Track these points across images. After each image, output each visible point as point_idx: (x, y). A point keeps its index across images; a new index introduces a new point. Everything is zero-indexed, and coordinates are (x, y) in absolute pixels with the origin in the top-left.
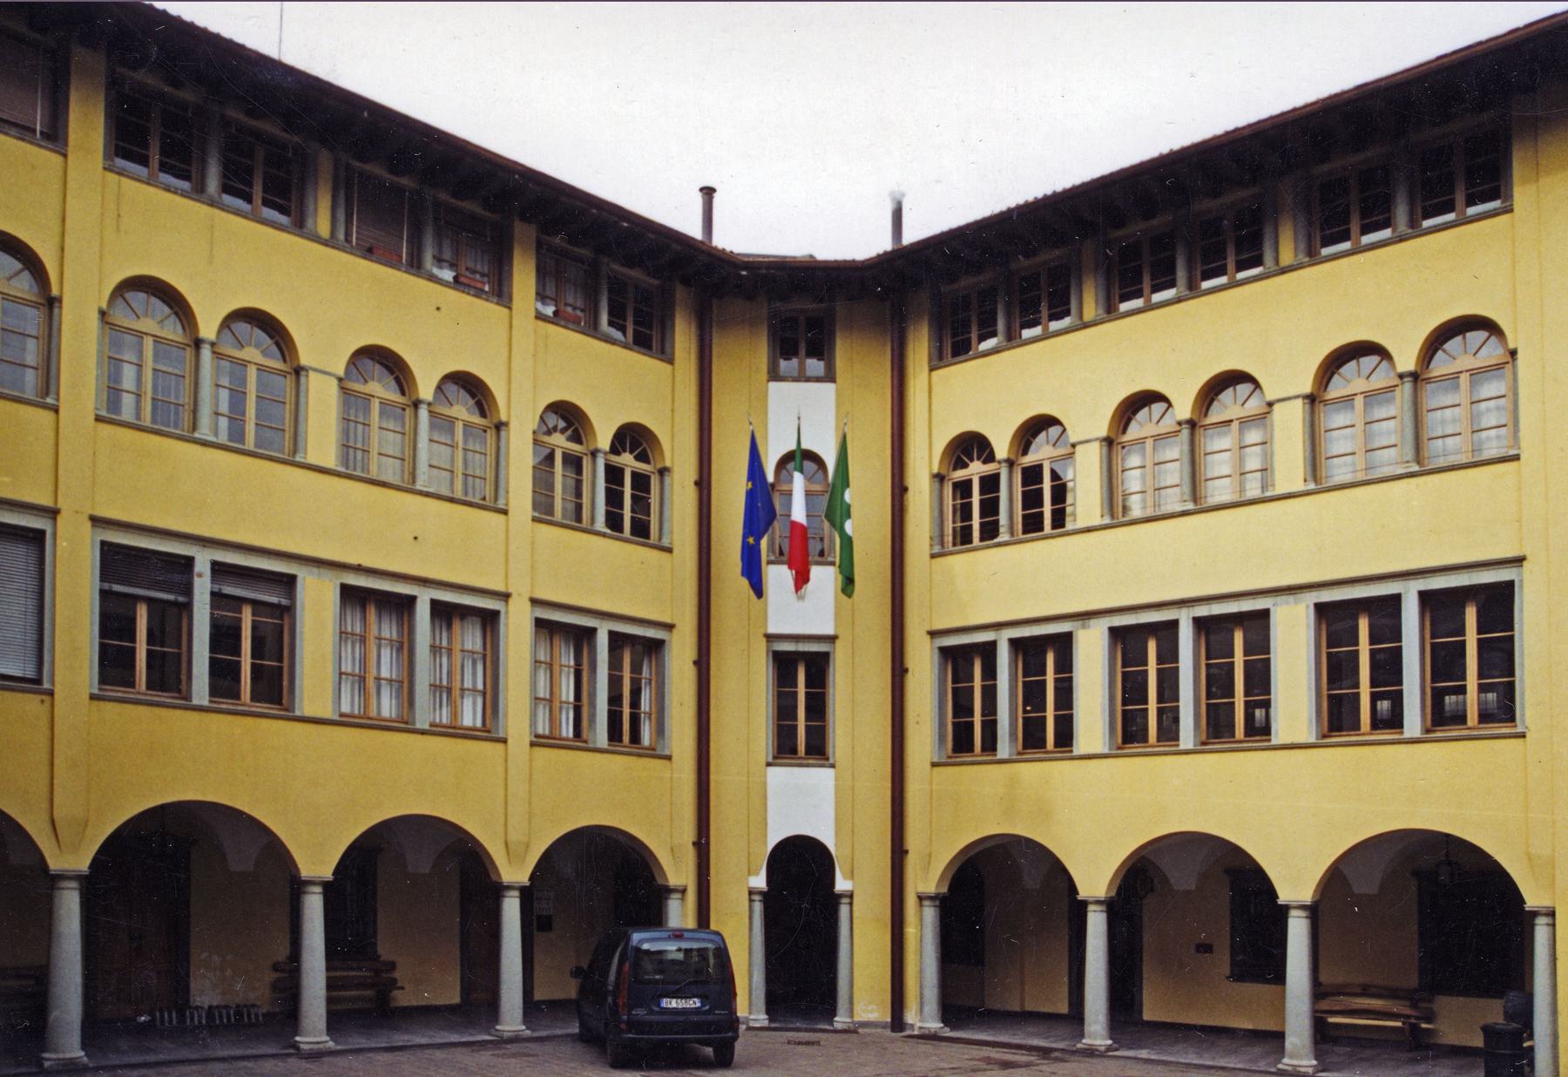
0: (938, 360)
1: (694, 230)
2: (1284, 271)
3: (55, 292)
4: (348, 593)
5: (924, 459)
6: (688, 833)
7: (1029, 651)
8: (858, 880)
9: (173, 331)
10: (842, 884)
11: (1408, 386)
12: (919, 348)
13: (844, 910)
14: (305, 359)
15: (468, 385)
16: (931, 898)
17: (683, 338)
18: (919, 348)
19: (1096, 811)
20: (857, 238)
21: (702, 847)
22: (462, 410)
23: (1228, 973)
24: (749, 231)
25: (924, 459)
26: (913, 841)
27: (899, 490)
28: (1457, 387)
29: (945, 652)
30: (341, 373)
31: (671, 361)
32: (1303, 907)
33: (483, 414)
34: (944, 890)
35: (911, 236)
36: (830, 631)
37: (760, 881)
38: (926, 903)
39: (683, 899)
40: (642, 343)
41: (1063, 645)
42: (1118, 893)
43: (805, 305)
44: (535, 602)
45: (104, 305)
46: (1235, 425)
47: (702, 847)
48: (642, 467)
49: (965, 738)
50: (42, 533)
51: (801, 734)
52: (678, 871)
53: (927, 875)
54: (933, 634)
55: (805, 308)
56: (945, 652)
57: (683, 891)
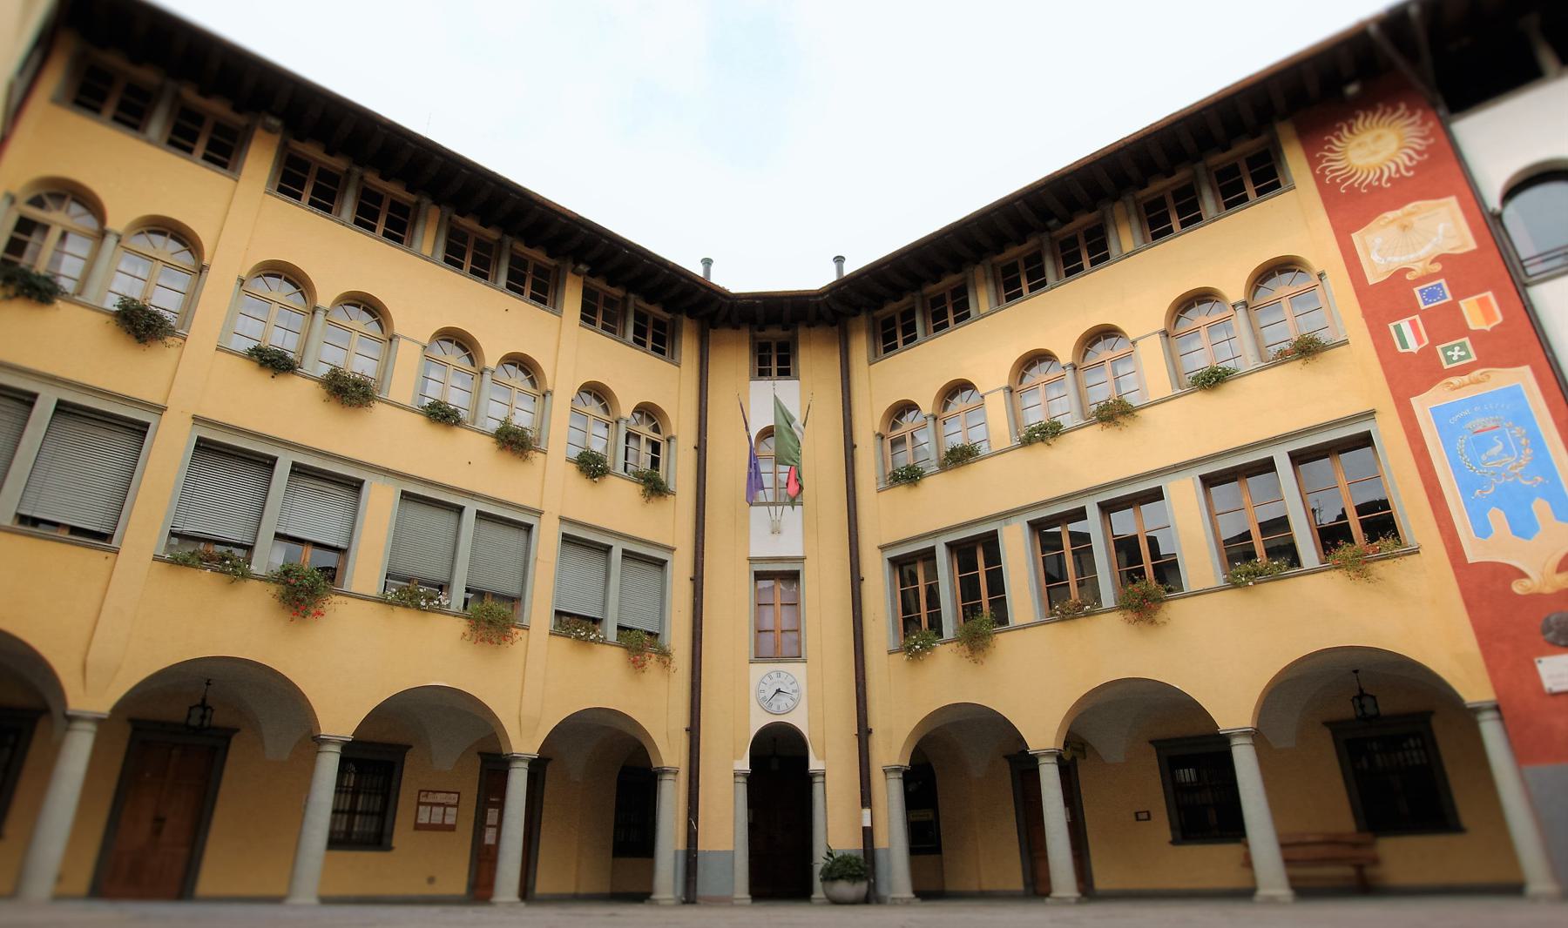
0: (874, 358)
1: (698, 270)
2: (1128, 255)
3: (206, 262)
4: (406, 496)
5: (869, 421)
6: (682, 719)
7: (963, 551)
8: (830, 760)
9: (296, 300)
10: (814, 764)
11: (1241, 311)
12: (860, 348)
13: (818, 789)
14: (398, 329)
15: (523, 364)
16: (897, 770)
17: (688, 349)
18: (860, 348)
19: (1038, 677)
20: (814, 276)
21: (694, 731)
22: (518, 379)
23: (1169, 838)
24: (735, 278)
25: (869, 421)
26: (876, 720)
27: (850, 447)
28: (1281, 308)
29: (894, 562)
30: (426, 342)
31: (678, 365)
32: (1245, 734)
33: (534, 385)
34: (907, 763)
35: (849, 269)
36: (800, 554)
37: (744, 765)
38: (891, 775)
39: (666, 665)
40: (659, 351)
41: (990, 543)
42: (1066, 744)
43: (774, 333)
44: (562, 520)
45: (244, 275)
46: (1108, 364)
47: (694, 731)
48: (655, 436)
49: (917, 625)
50: (147, 425)
51: (777, 644)
52: (670, 752)
53: (891, 750)
54: (883, 548)
55: (776, 328)
56: (894, 562)
57: (676, 773)
